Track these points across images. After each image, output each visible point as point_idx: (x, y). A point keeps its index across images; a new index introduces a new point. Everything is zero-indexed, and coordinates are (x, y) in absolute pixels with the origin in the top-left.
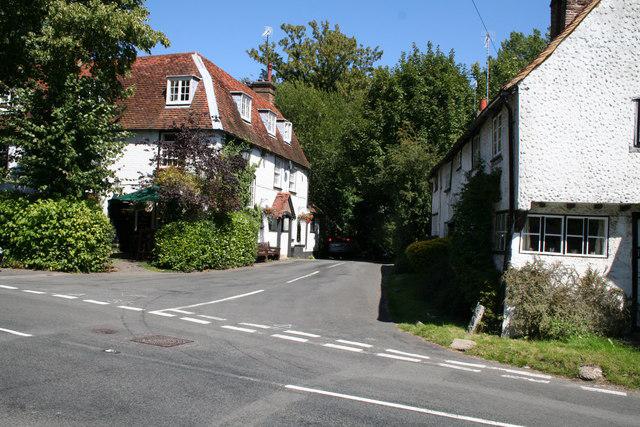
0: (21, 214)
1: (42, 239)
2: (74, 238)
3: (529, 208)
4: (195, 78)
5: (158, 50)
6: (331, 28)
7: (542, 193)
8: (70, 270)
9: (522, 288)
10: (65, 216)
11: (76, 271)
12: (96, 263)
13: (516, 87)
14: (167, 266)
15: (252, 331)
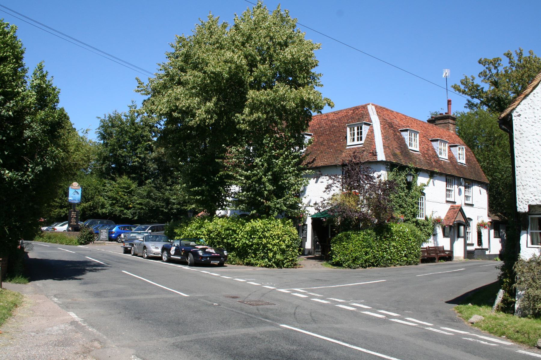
0: (241, 230)
1: (252, 245)
2: (272, 244)
3: (527, 210)
4: (365, 124)
5: (326, 110)
6: (526, 54)
7: (536, 197)
8: (270, 266)
9: (528, 276)
10: (266, 230)
11: (274, 267)
12: (288, 262)
13: (510, 115)
14: (338, 264)
15: (408, 319)
